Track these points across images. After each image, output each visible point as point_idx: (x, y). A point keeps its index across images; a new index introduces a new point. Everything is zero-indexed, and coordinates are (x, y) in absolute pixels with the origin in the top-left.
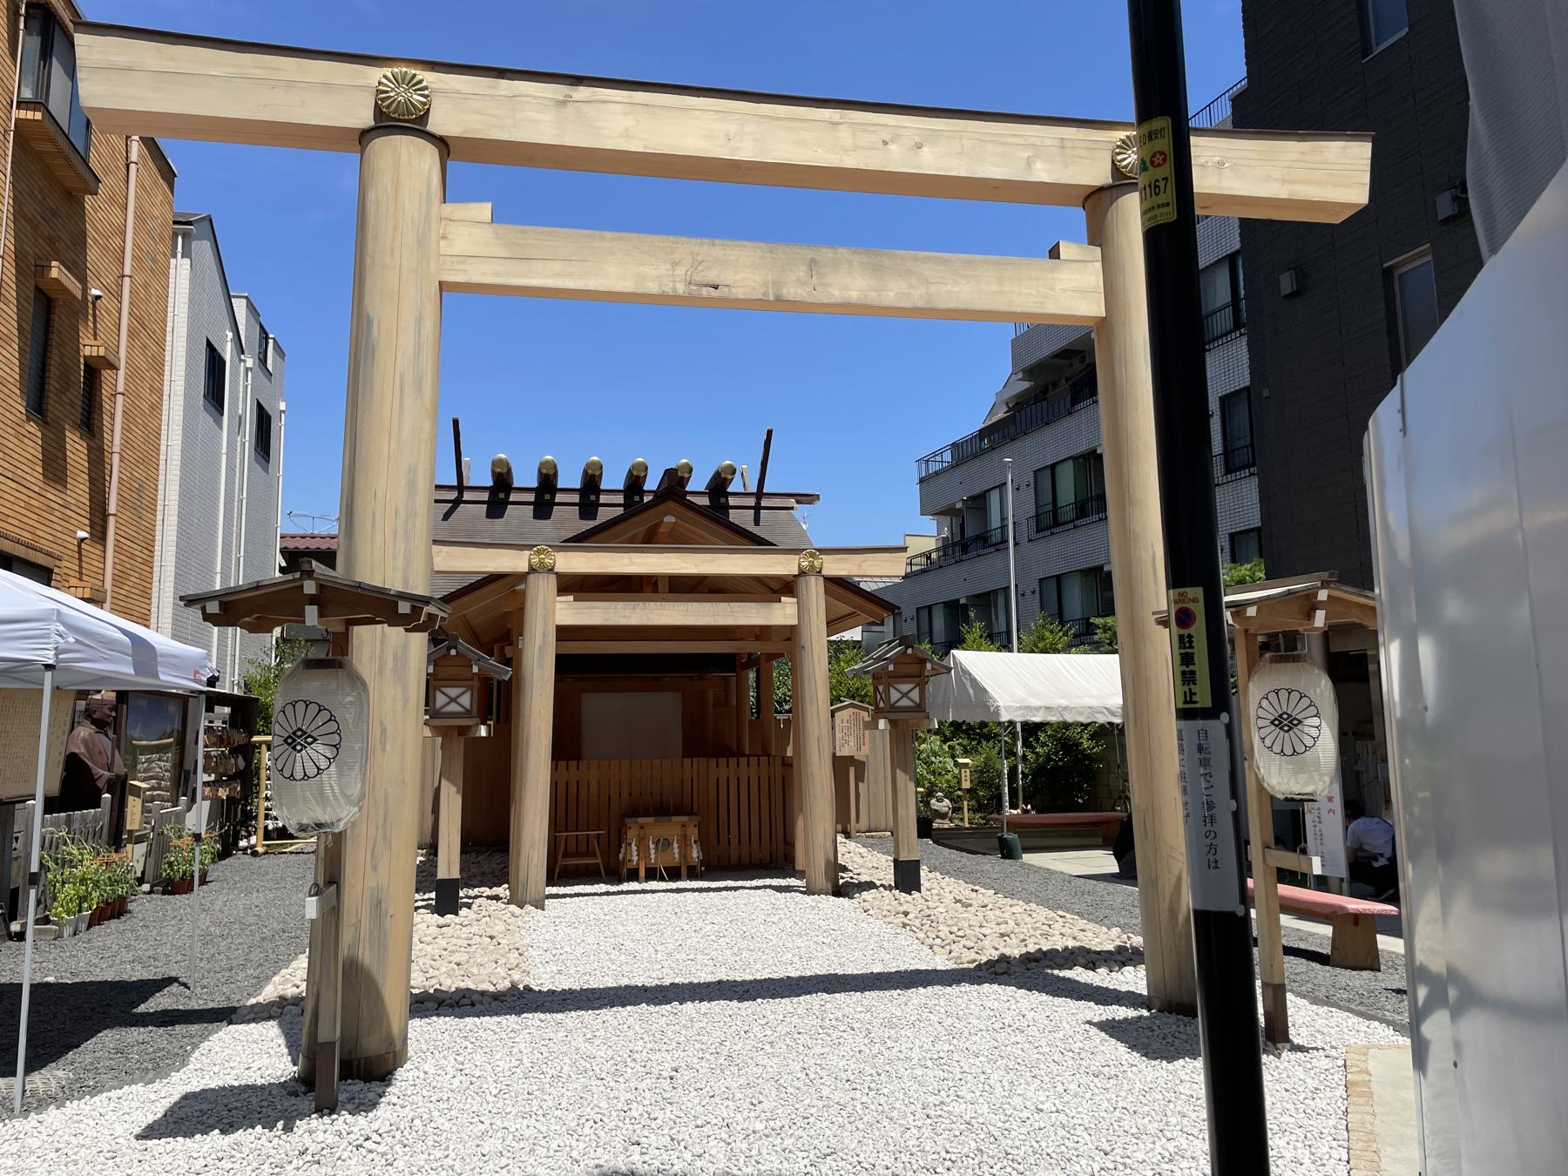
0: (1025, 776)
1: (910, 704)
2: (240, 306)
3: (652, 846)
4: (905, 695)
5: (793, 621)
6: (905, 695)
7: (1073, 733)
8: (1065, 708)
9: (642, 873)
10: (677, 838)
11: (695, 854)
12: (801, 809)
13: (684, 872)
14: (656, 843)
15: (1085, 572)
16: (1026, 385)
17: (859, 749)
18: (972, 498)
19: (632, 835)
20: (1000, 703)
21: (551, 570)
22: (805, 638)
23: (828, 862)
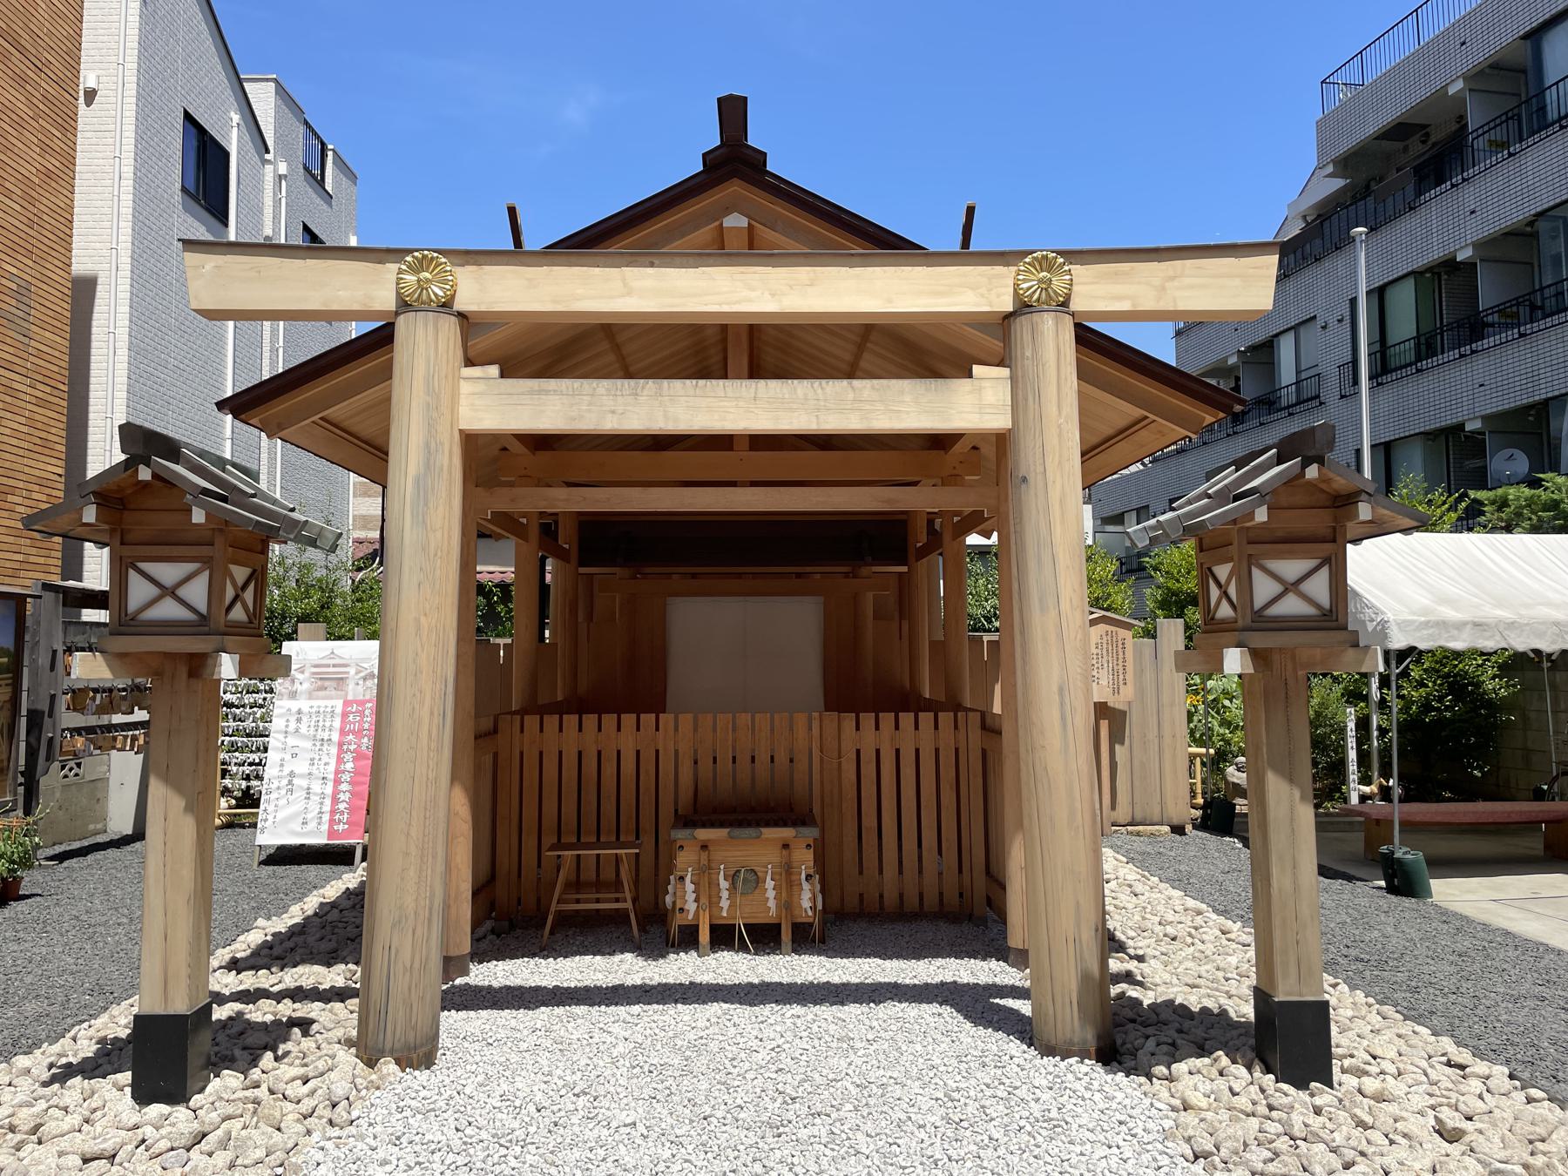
0: (1383, 732)
1: (1308, 610)
2: (263, 97)
3: (724, 884)
4: (1292, 587)
5: (1000, 421)
6: (1292, 587)
7: (1470, 666)
8: (1511, 625)
9: (704, 936)
10: (770, 869)
11: (807, 900)
12: (1020, 825)
13: (786, 935)
14: (733, 878)
15: (1430, 436)
16: (1339, 183)
17: (1116, 691)
18: (1253, 349)
19: (686, 860)
20: (1390, 616)
21: (446, 305)
22: (1028, 458)
23: (1085, 978)
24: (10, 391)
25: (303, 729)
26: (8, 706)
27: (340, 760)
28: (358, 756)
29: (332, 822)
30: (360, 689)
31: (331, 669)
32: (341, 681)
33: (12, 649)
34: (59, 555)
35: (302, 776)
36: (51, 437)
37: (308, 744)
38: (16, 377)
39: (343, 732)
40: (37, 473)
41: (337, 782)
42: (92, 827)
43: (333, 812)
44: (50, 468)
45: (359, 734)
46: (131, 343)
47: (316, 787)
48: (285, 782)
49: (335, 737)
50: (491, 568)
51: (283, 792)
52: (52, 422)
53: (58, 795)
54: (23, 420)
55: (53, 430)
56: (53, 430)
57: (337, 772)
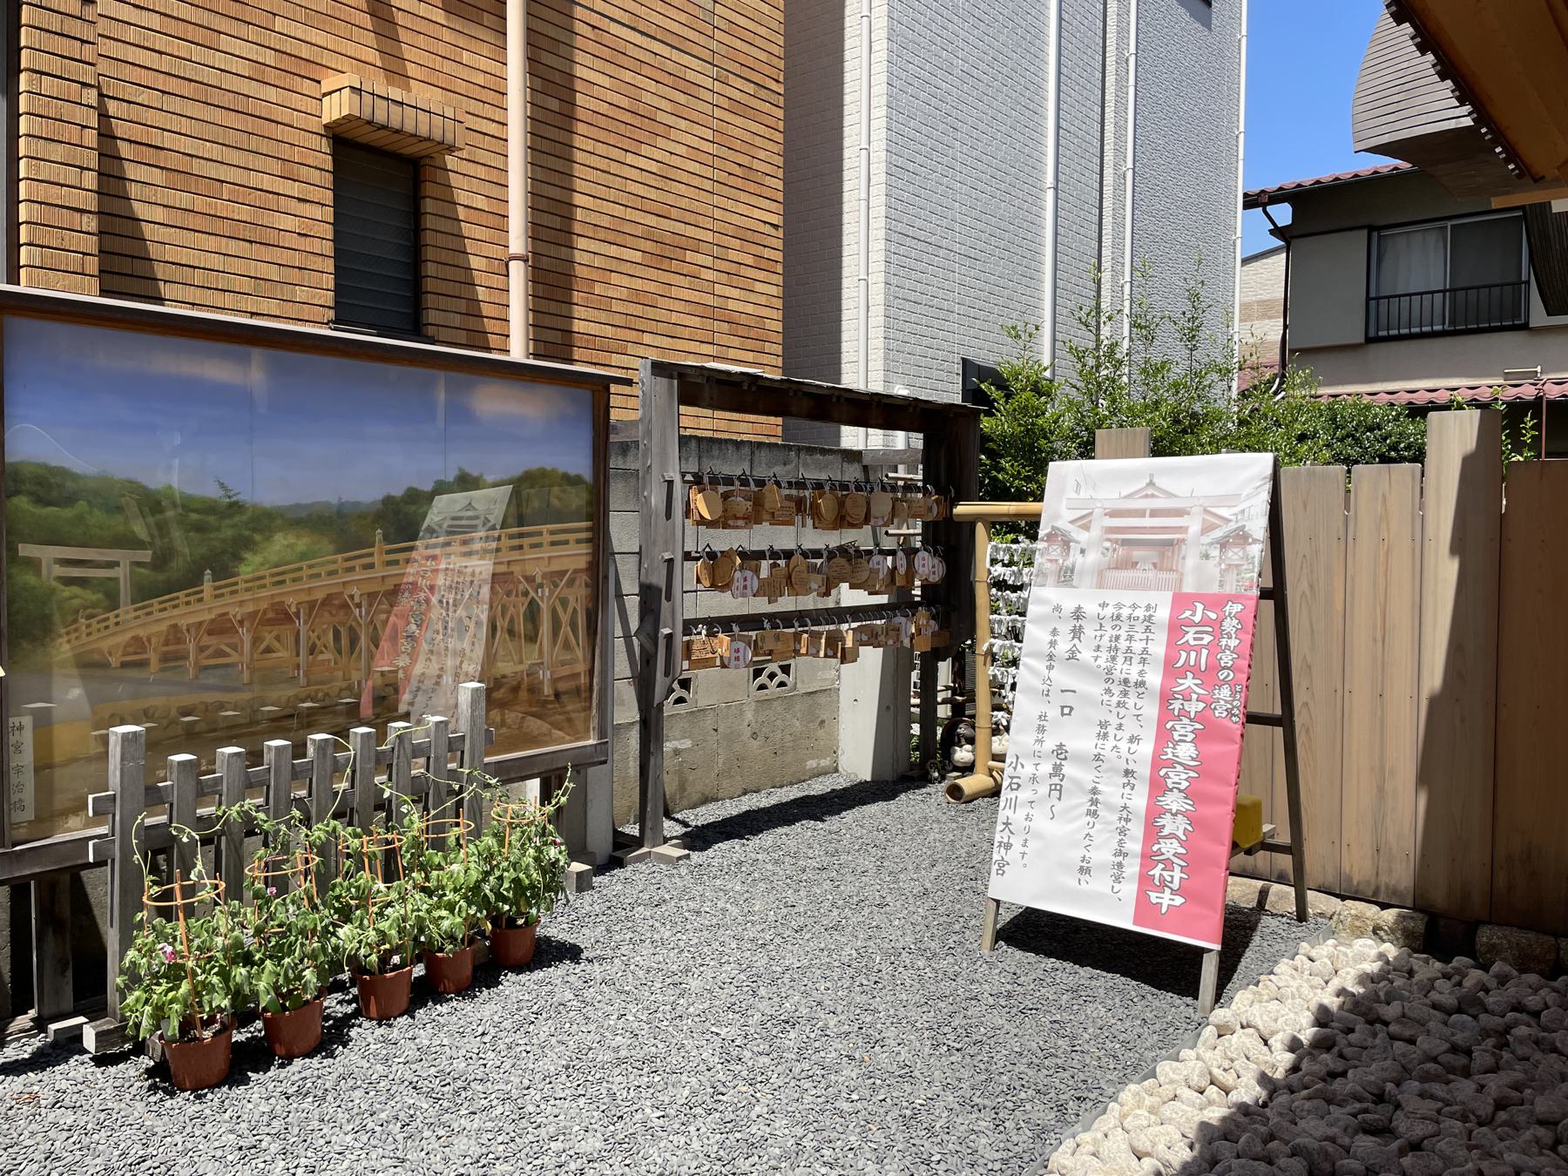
24: (682, 85)
25: (1086, 655)
26: (584, 577)
27: (1164, 736)
28: (1207, 732)
29: (1145, 880)
30: (1212, 568)
31: (1148, 522)
32: (1167, 549)
33: (587, 475)
34: (779, 349)
35: (1080, 759)
36: (756, 164)
37: (1096, 689)
38: (695, 63)
39: (1171, 670)
40: (736, 219)
41: (1158, 787)
42: (812, 764)
43: (1148, 858)
44: (757, 214)
45: (1209, 674)
46: (891, 29)
47: (1112, 791)
48: (1046, 768)
49: (1155, 679)
50: (1454, 382)
51: (1043, 789)
52: (759, 141)
53: (749, 716)
54: (709, 134)
55: (762, 155)
56: (762, 155)
57: (1157, 763)
